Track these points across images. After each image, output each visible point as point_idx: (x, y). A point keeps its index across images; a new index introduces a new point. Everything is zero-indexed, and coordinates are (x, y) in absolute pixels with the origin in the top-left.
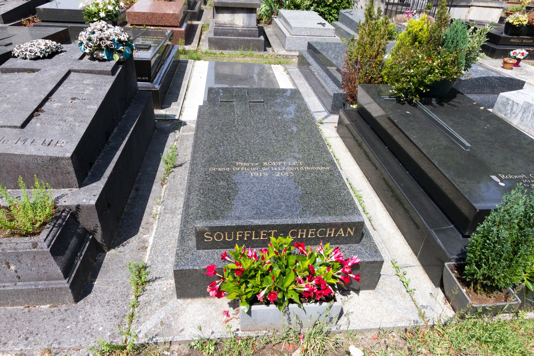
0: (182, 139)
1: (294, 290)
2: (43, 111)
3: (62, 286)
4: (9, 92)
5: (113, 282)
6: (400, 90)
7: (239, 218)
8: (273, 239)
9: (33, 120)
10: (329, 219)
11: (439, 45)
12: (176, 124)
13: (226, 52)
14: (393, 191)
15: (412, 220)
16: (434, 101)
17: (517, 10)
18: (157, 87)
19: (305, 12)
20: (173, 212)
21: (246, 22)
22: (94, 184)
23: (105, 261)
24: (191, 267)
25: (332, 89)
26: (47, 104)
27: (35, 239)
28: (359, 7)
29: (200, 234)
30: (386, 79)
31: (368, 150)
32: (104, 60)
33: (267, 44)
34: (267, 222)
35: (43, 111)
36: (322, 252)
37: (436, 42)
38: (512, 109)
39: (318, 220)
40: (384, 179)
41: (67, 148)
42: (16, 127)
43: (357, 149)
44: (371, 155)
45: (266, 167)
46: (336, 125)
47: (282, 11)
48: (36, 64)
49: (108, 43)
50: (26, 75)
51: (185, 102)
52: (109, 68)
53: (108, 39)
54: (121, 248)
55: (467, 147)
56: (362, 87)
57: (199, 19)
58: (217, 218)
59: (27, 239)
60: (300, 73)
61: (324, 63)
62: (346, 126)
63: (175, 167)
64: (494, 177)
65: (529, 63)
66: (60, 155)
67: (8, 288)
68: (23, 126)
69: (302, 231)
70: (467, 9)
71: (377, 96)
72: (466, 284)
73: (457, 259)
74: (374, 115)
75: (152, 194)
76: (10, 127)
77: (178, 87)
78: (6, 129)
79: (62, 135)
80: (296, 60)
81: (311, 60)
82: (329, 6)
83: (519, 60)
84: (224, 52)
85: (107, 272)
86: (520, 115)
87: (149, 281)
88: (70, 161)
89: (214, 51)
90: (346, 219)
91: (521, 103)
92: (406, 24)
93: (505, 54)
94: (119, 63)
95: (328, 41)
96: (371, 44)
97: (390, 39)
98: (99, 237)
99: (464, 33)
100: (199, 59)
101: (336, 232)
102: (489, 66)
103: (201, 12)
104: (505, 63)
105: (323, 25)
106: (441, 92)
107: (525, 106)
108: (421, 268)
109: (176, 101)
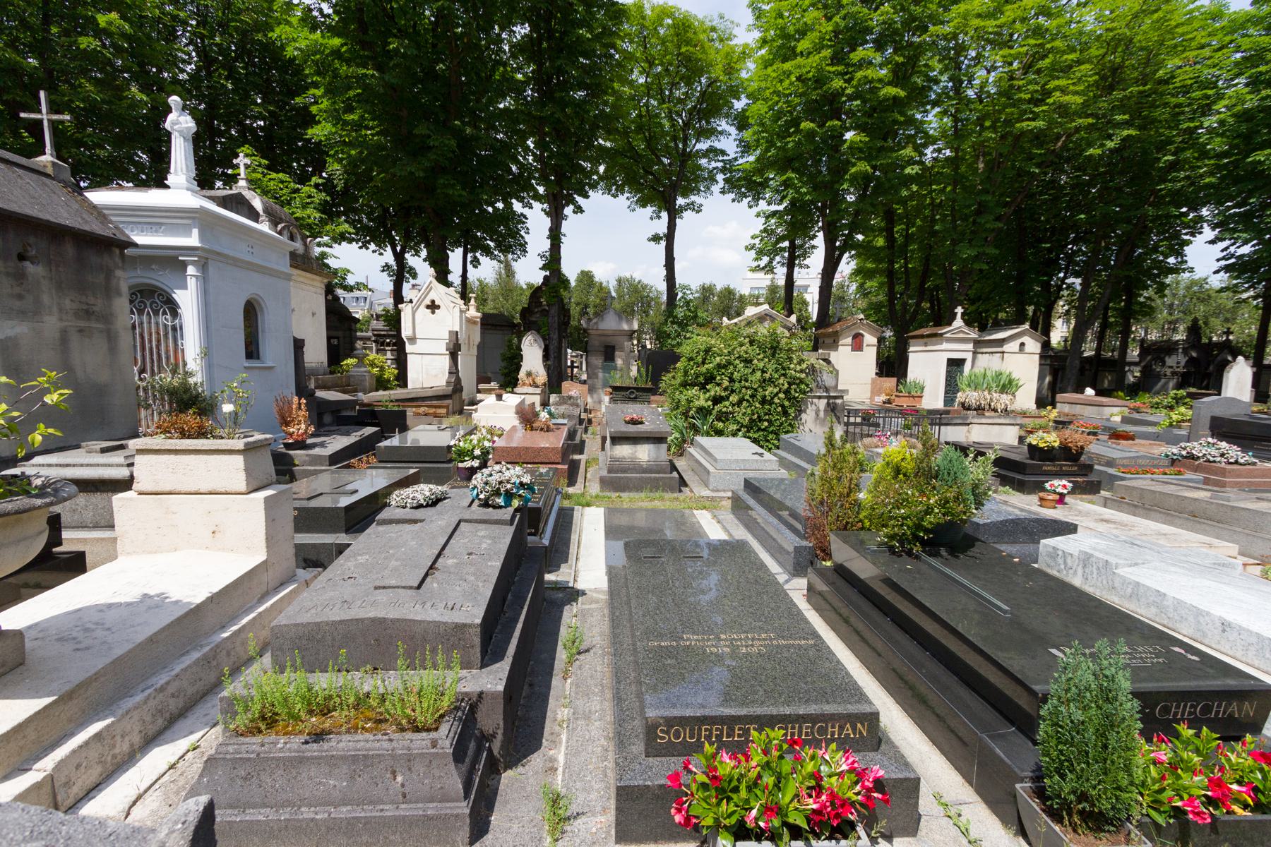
0: (583, 615)
1: (796, 809)
2: (437, 569)
3: (460, 811)
4: (391, 548)
5: (517, 818)
6: (892, 537)
7: (703, 706)
8: (754, 734)
9: (429, 579)
10: (829, 709)
11: (931, 478)
12: (573, 594)
13: (625, 495)
14: (912, 688)
15: (952, 731)
16: (943, 552)
17: (1041, 428)
18: (546, 542)
19: (731, 439)
20: (587, 717)
21: (653, 455)
22: (497, 665)
23: (501, 787)
24: (641, 783)
25: (790, 541)
26: (440, 560)
27: (433, 735)
28: (807, 429)
29: (651, 730)
30: (867, 524)
31: (860, 626)
32: (501, 507)
33: (683, 482)
34: (743, 712)
35: (437, 569)
36: (827, 757)
37: (926, 475)
38: (1065, 563)
39: (813, 709)
40: (894, 670)
41: (474, 613)
42: (411, 588)
43: (844, 627)
44: (867, 635)
45: (726, 640)
46: (805, 592)
47: (698, 438)
48: (419, 514)
49: (509, 486)
50: (407, 527)
51: (580, 564)
52: (508, 517)
53: (508, 482)
54: (520, 769)
55: (1005, 612)
56: (837, 535)
57: (581, 453)
58: (674, 706)
59: (424, 734)
60: (736, 521)
61: (773, 506)
62: (820, 594)
63: (579, 653)
64: (1054, 651)
65: (1082, 500)
66: (468, 621)
67: (388, 814)
68: (419, 587)
69: (793, 728)
70: (965, 428)
71: (860, 546)
72: (1056, 816)
73: (1031, 778)
74: (862, 576)
75: (552, 692)
76: (404, 587)
77: (567, 543)
78: (400, 591)
79: (464, 598)
80: (728, 504)
81: (751, 502)
82: (764, 430)
83: (1062, 495)
84: (622, 494)
85: (507, 802)
86: (1080, 571)
87: (569, 819)
88: (479, 630)
89: (608, 494)
90: (853, 708)
91: (1076, 554)
92: (880, 450)
93: (1039, 487)
94: (517, 510)
95: (771, 476)
96: (839, 479)
97: (862, 471)
98: (496, 746)
99: (962, 462)
100: (588, 505)
101: (841, 728)
102: (1013, 504)
103: (583, 442)
104: (1041, 499)
105: (761, 455)
106: (950, 539)
107: (1082, 557)
108: (984, 806)
109: (566, 561)
